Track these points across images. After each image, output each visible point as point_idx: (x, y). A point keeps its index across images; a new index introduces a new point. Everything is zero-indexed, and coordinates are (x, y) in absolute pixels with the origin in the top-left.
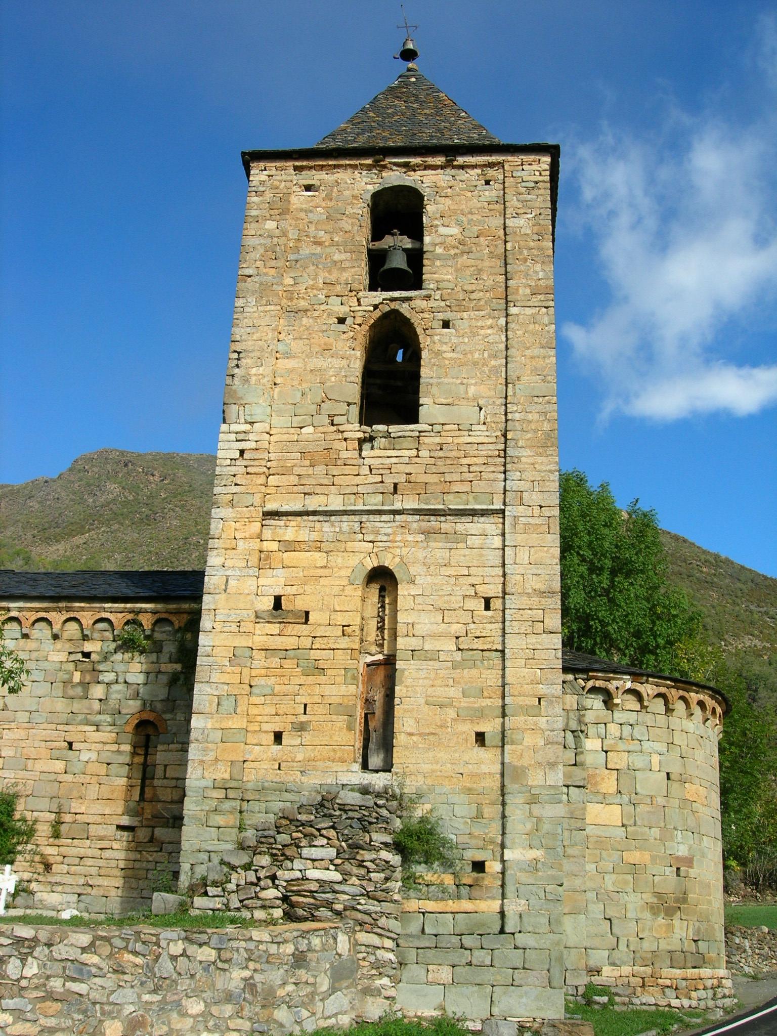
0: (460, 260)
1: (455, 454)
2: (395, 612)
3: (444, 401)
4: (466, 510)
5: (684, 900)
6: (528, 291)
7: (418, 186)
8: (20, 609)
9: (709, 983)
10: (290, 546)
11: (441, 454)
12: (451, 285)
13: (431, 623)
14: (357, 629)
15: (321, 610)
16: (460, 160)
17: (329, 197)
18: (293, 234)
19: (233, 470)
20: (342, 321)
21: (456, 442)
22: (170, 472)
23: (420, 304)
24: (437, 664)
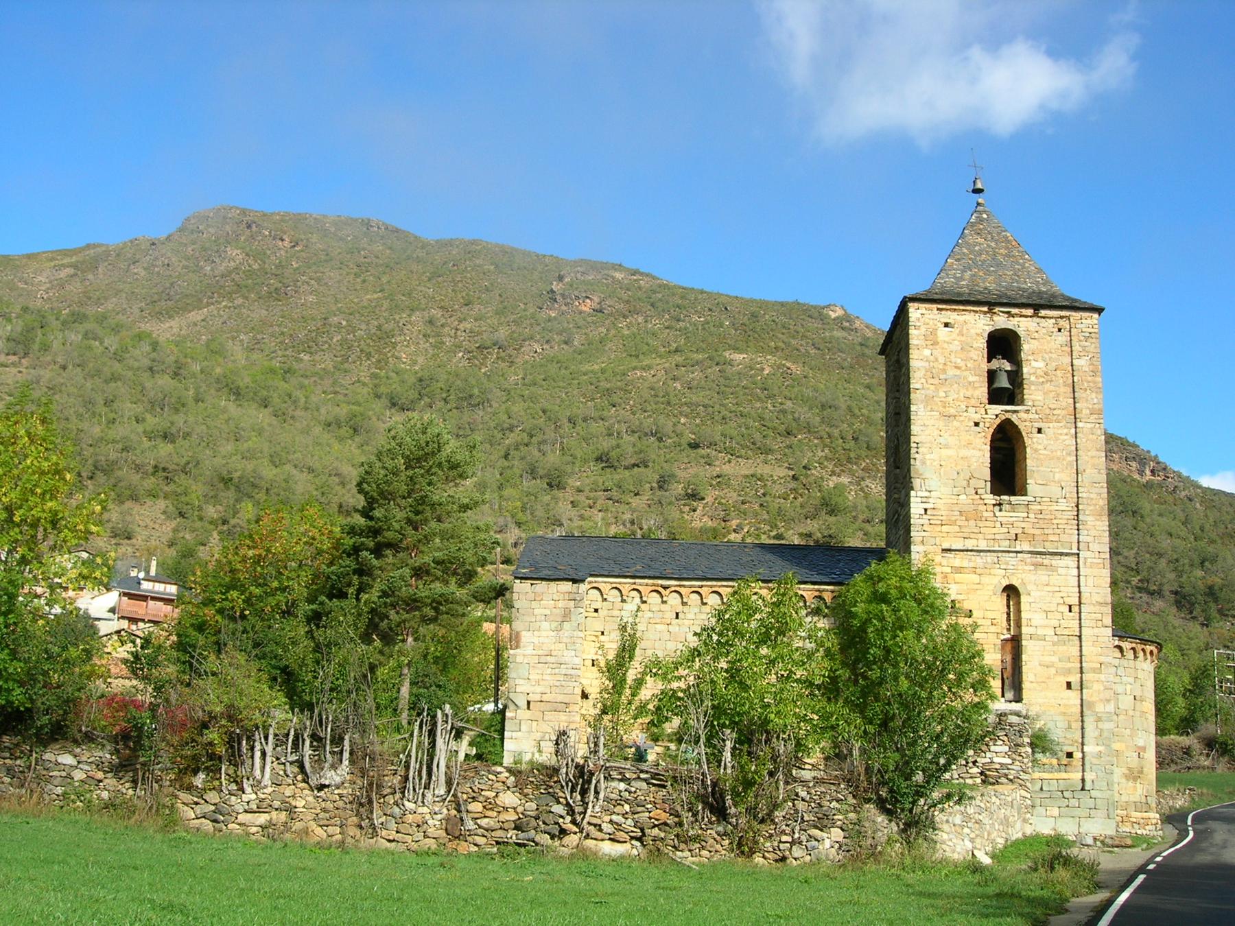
2: (1019, 611)
5: (1141, 772)
10: (958, 570)
16: (1043, 313)
18: (941, 360)
19: (921, 521)
20: (977, 424)
22: (303, 237)
23: (1022, 415)
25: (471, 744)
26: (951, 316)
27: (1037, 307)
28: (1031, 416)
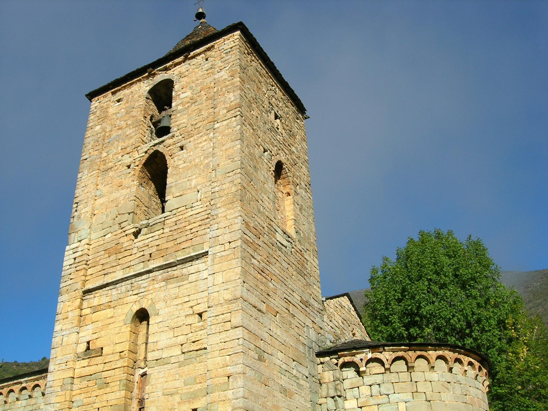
0: (190, 109)
3: (178, 194)
4: (187, 258)
6: (225, 111)
12: (185, 125)
13: (167, 339)
15: (109, 345)
20: (129, 167)
21: (184, 217)
24: (169, 366)
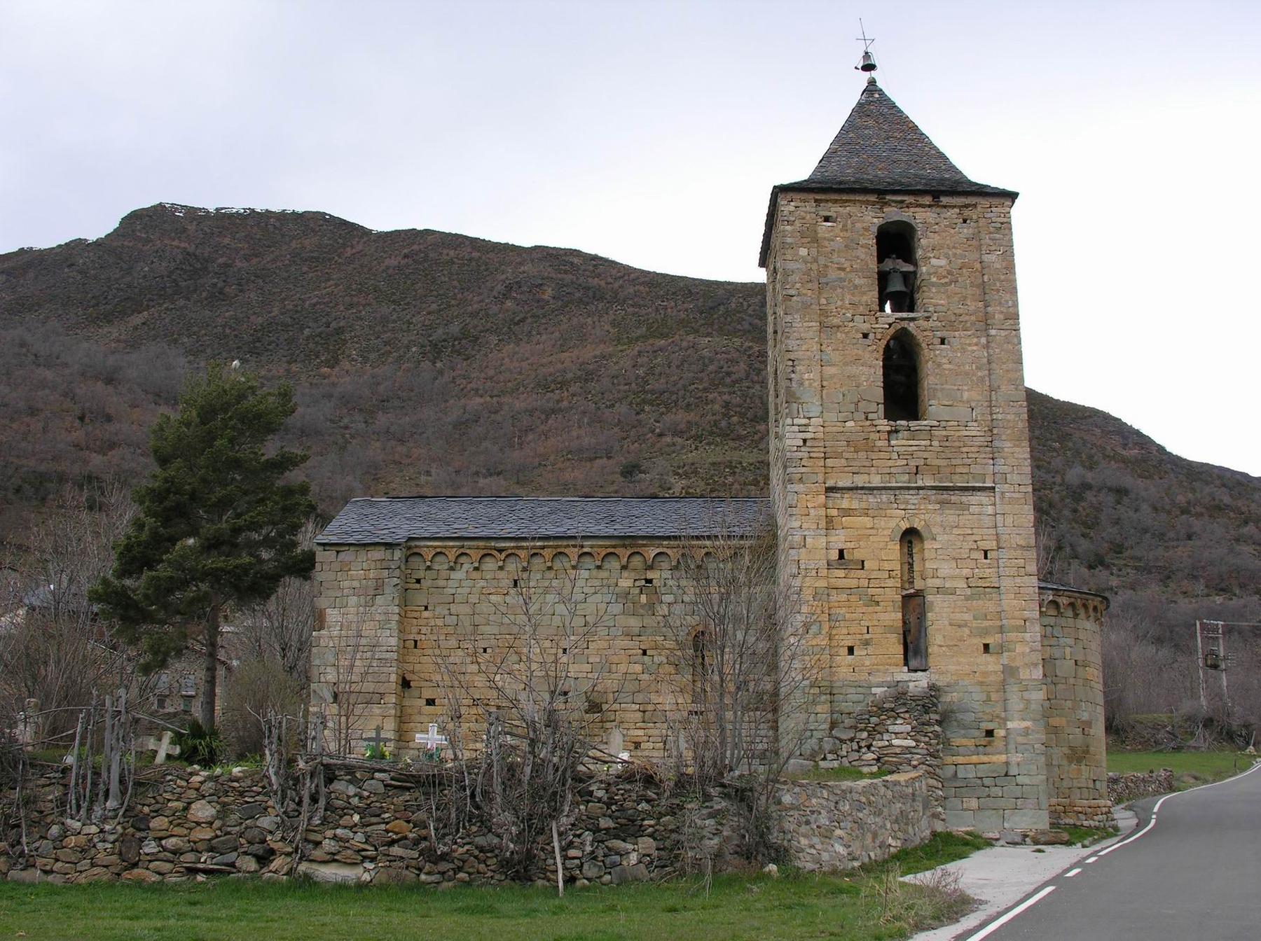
1: (957, 444)
5: (1088, 752)
6: (1002, 317)
7: (913, 222)
8: (592, 547)
9: (1104, 810)
10: (847, 512)
11: (947, 444)
14: (899, 572)
16: (945, 200)
17: (844, 229)
20: (865, 336)
25: (173, 742)
26: (833, 210)
27: (936, 194)
28: (931, 324)
